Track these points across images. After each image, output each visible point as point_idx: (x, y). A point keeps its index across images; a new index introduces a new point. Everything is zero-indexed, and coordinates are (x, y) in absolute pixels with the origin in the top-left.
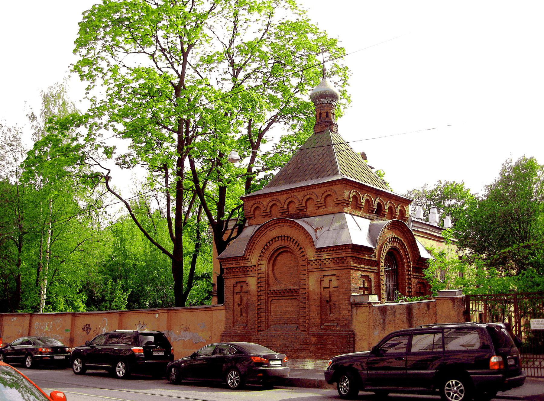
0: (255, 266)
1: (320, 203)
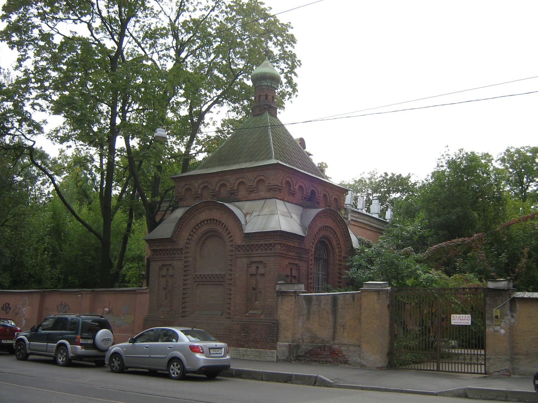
0: (182, 249)
1: (252, 187)
